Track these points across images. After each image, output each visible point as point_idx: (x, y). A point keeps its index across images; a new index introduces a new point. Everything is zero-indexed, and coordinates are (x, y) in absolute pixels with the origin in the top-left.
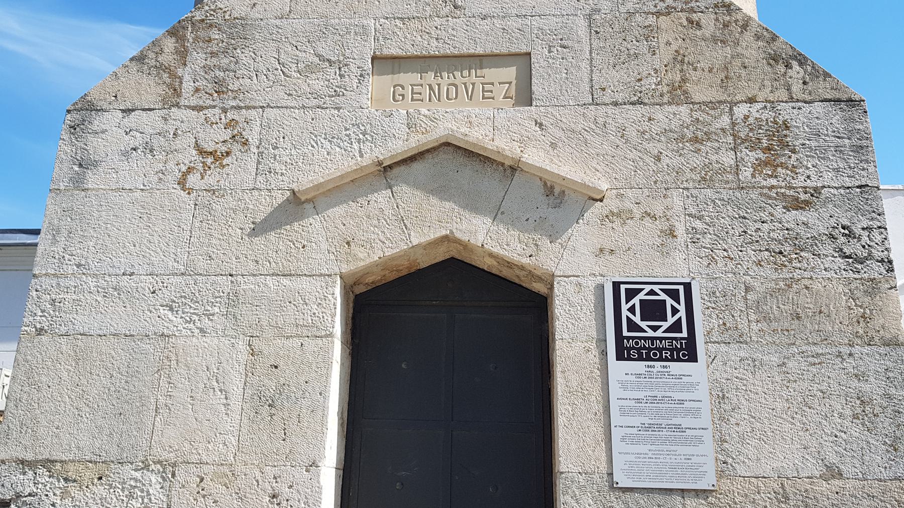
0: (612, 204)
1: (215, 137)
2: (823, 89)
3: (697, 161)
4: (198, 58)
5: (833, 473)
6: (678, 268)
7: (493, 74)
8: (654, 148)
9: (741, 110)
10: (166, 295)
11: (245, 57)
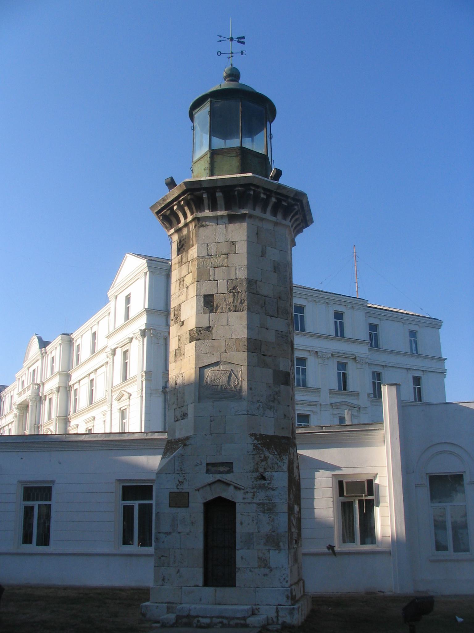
1: (181, 479)
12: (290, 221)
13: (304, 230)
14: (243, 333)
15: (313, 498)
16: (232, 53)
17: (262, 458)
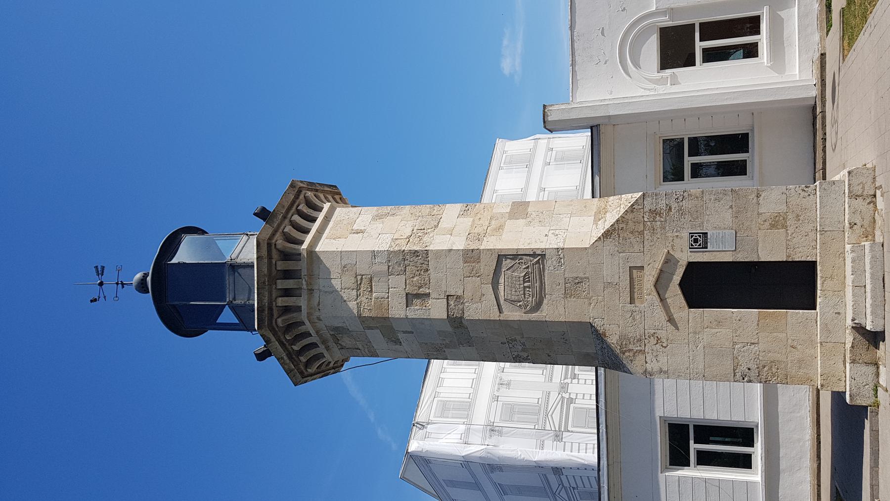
0: (670, 248)
1: (653, 341)
2: (641, 201)
3: (659, 230)
4: (631, 347)
5: (731, 207)
6: (685, 235)
7: (635, 276)
8: (655, 239)
9: (646, 219)
10: (694, 348)
11: (630, 335)
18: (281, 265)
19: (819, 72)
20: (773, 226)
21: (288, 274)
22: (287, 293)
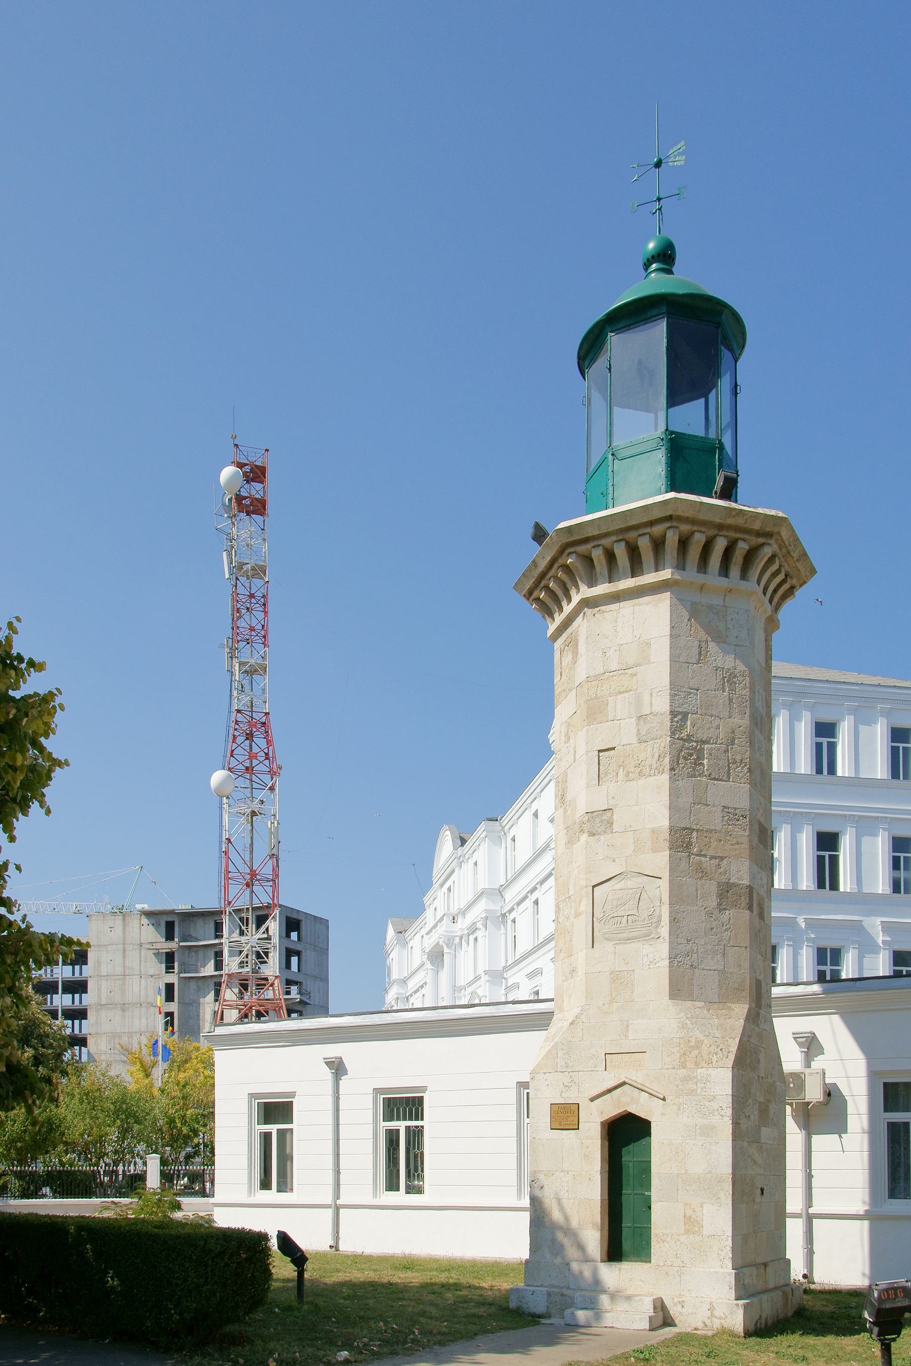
12: (759, 583)
13: (258, 1230)
14: (662, 820)
15: (621, 1195)
16: (659, 199)
17: (693, 1044)
18: (644, 544)
19: (333, 1228)
20: (688, 1219)
21: (634, 552)
22: (610, 556)
